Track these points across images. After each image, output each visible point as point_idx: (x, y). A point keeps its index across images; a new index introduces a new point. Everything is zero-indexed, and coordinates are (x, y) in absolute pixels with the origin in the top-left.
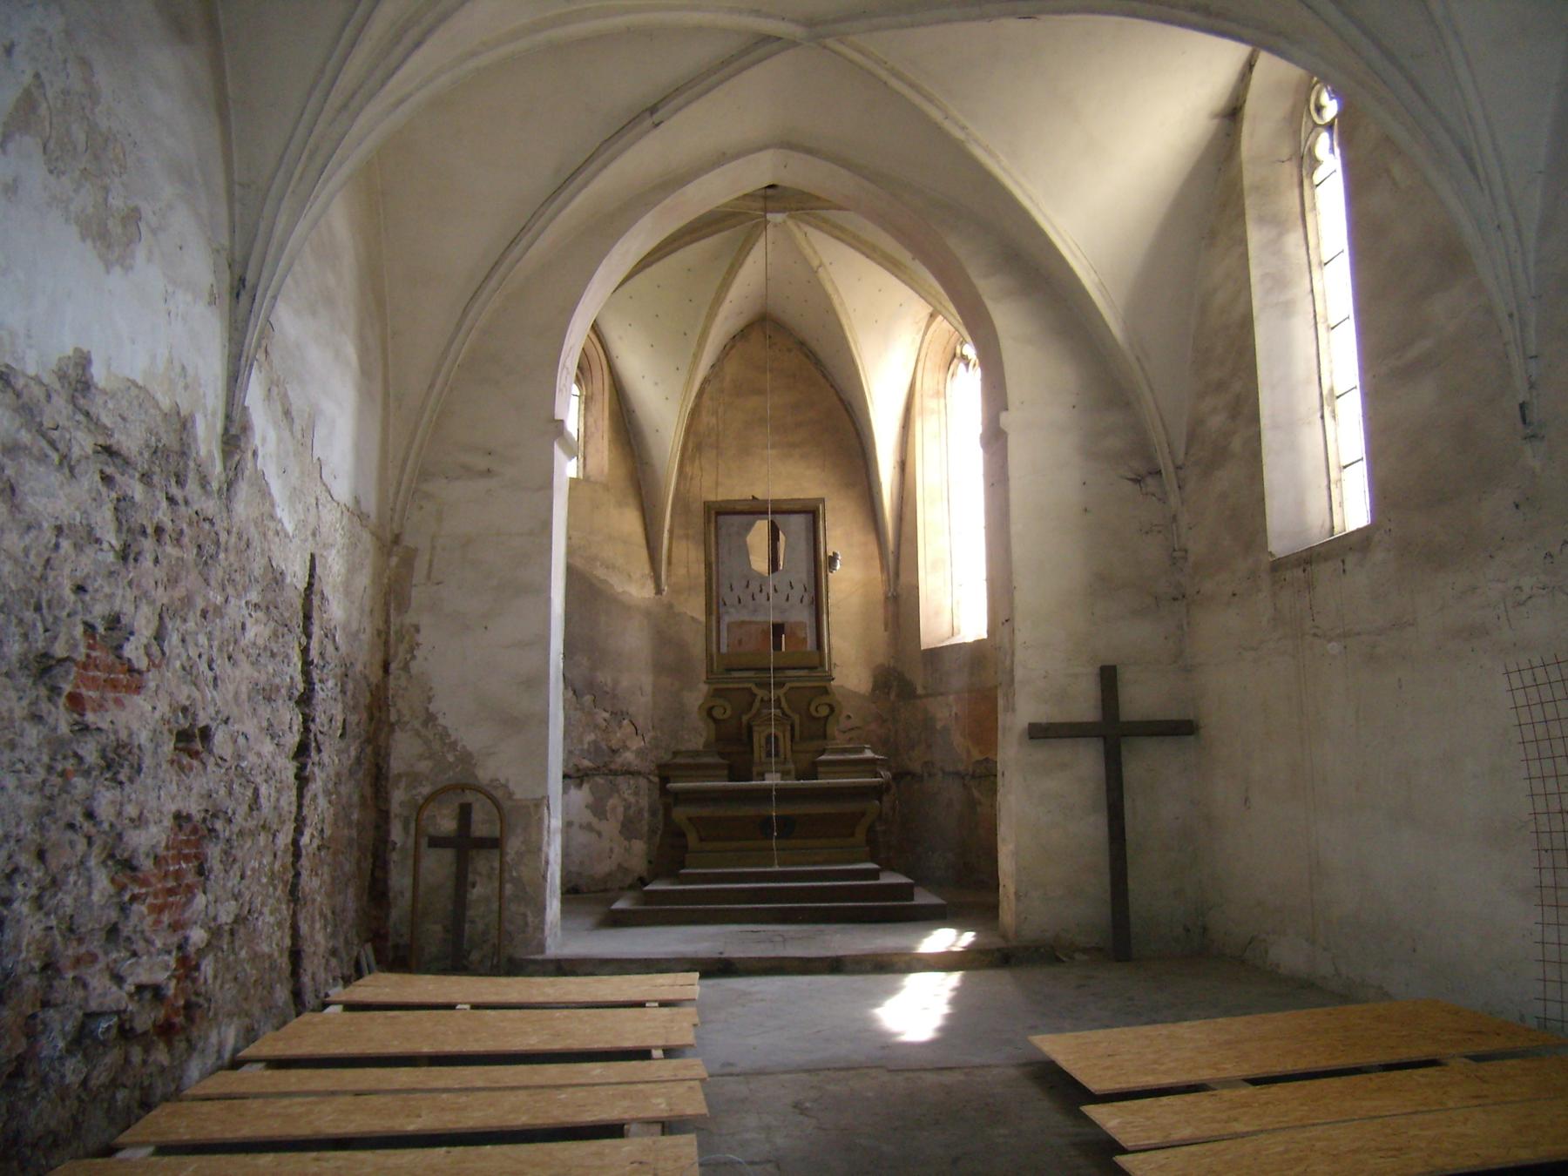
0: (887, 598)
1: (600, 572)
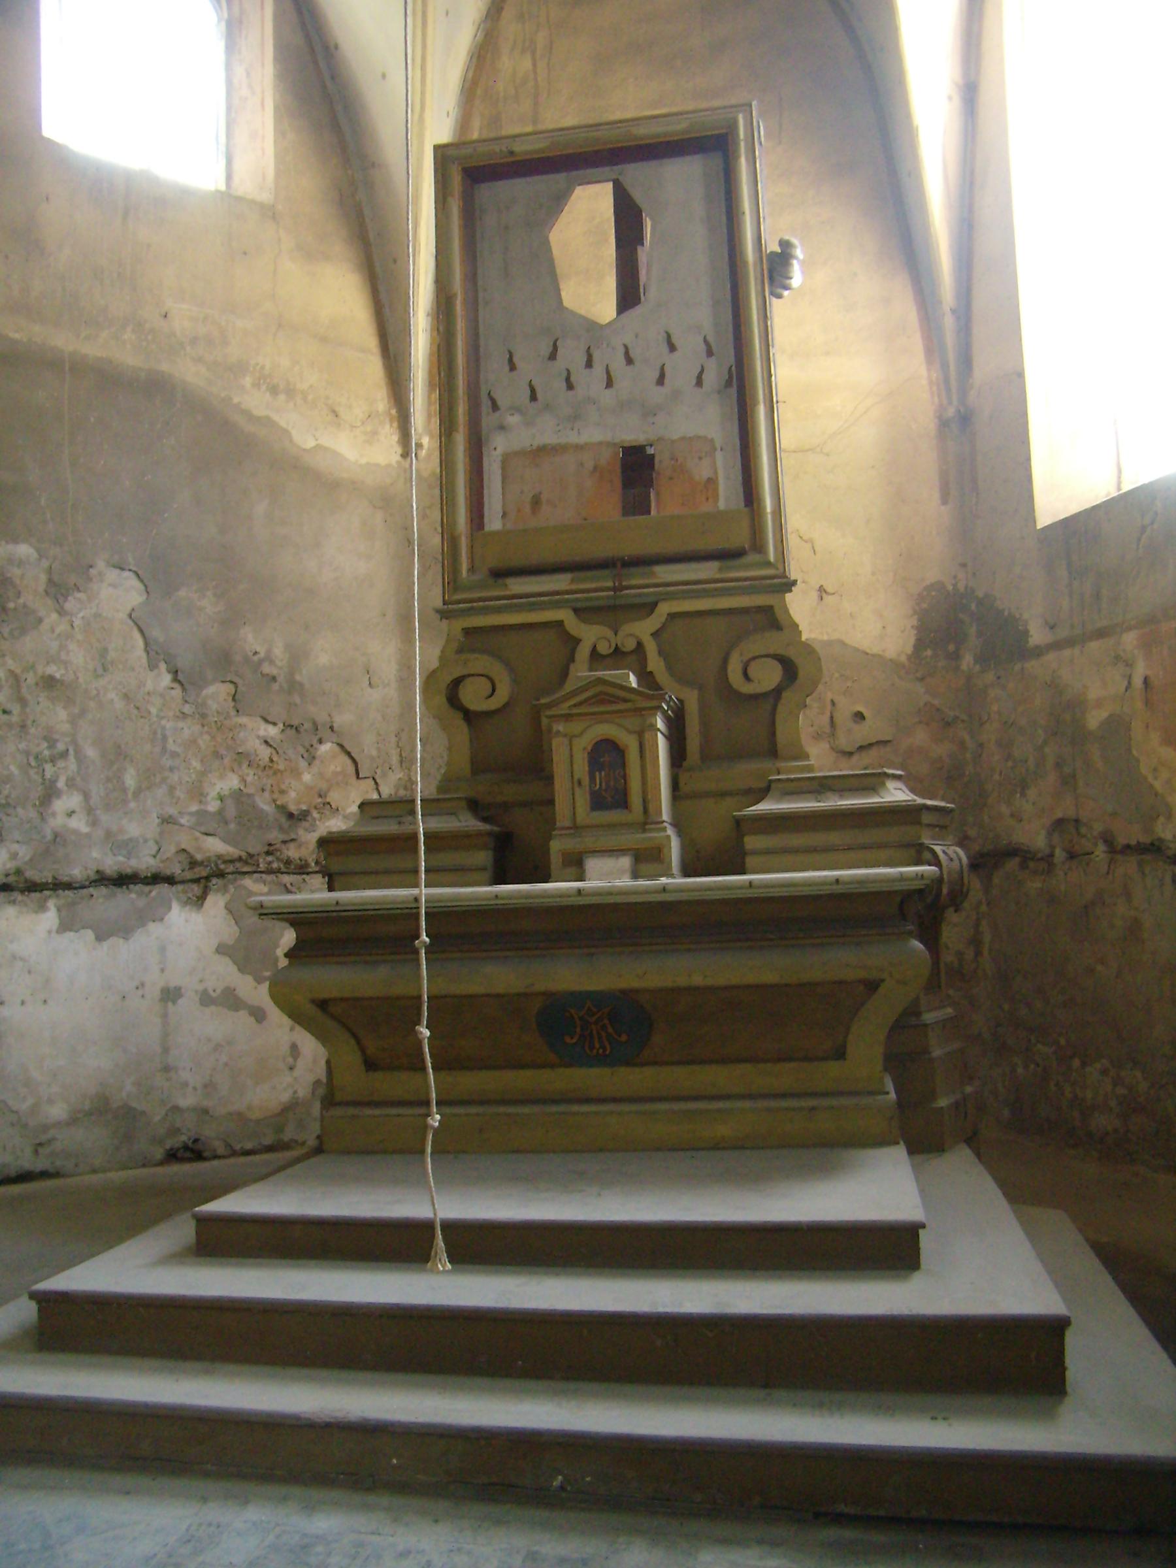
0: (943, 424)
1: (256, 402)
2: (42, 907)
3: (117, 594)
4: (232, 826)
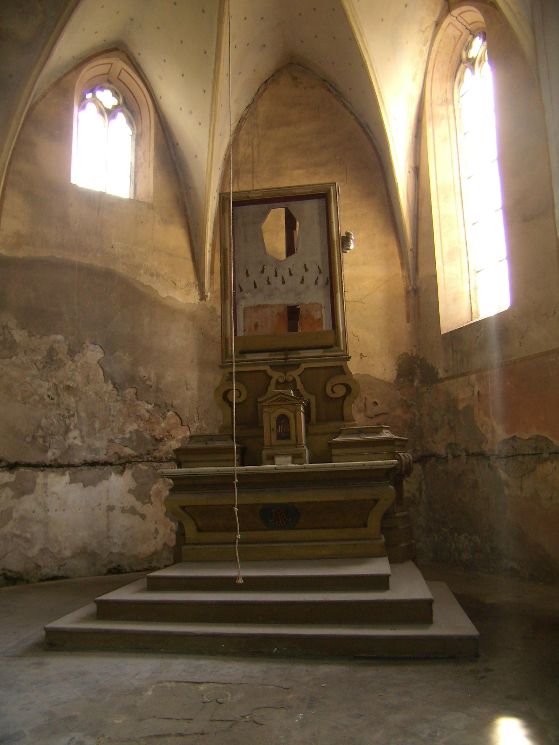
0: (408, 292)
1: (145, 279)
2: (63, 474)
3: (93, 354)
4: (135, 443)
